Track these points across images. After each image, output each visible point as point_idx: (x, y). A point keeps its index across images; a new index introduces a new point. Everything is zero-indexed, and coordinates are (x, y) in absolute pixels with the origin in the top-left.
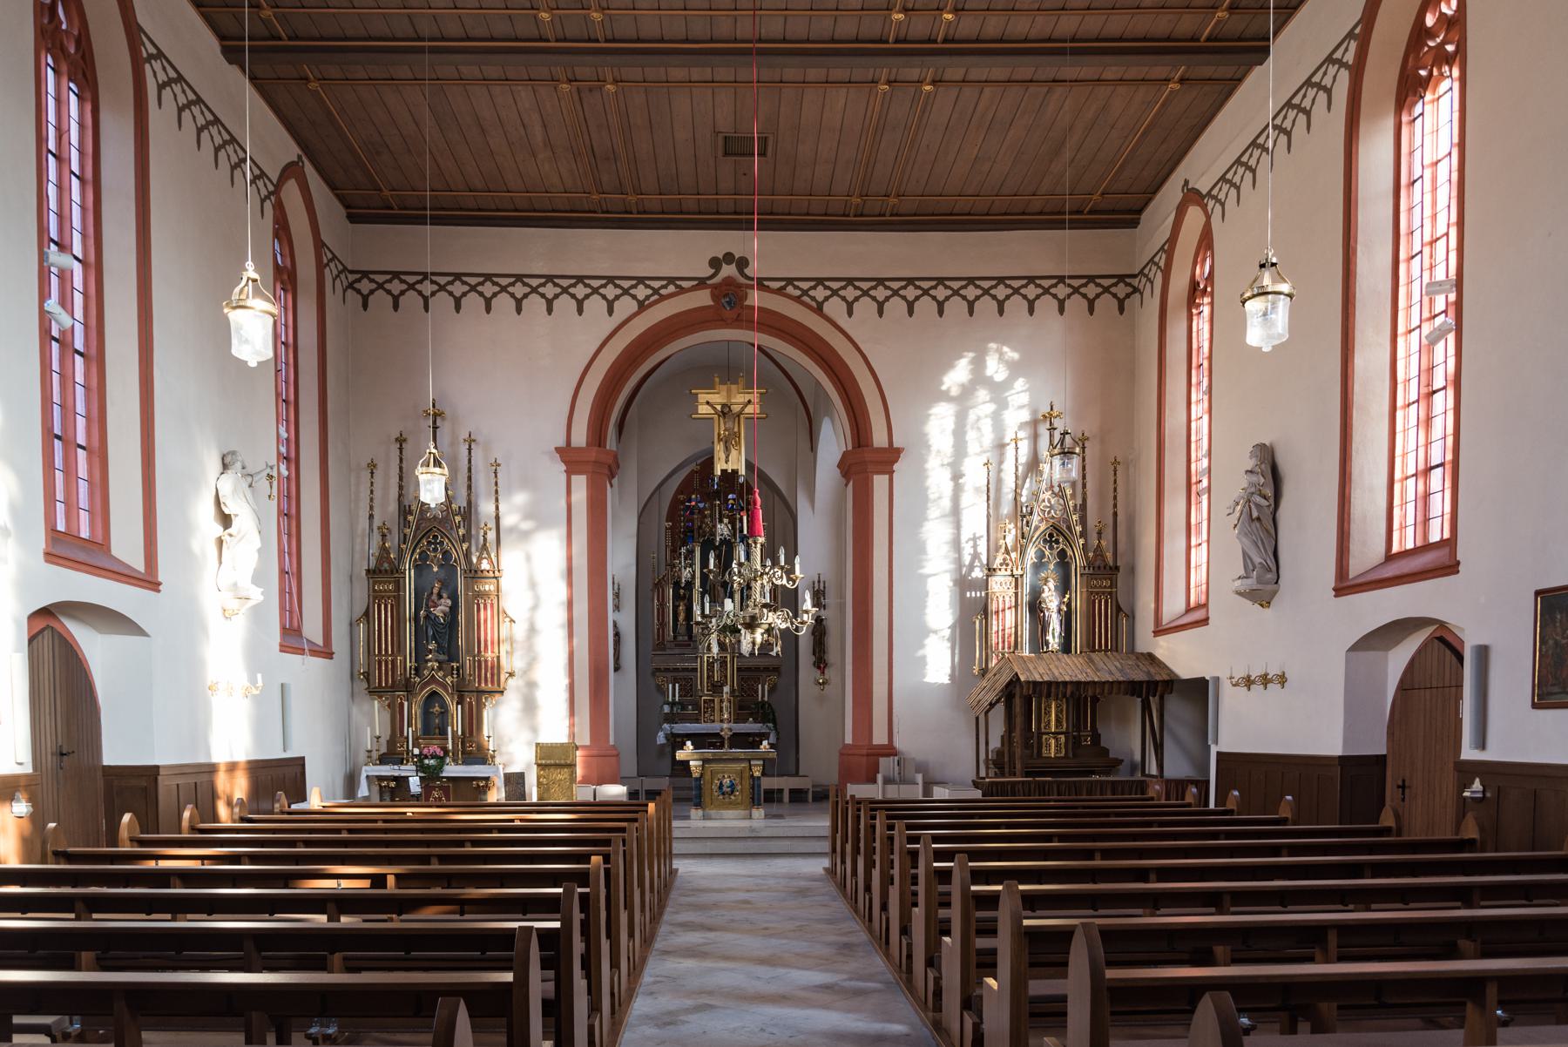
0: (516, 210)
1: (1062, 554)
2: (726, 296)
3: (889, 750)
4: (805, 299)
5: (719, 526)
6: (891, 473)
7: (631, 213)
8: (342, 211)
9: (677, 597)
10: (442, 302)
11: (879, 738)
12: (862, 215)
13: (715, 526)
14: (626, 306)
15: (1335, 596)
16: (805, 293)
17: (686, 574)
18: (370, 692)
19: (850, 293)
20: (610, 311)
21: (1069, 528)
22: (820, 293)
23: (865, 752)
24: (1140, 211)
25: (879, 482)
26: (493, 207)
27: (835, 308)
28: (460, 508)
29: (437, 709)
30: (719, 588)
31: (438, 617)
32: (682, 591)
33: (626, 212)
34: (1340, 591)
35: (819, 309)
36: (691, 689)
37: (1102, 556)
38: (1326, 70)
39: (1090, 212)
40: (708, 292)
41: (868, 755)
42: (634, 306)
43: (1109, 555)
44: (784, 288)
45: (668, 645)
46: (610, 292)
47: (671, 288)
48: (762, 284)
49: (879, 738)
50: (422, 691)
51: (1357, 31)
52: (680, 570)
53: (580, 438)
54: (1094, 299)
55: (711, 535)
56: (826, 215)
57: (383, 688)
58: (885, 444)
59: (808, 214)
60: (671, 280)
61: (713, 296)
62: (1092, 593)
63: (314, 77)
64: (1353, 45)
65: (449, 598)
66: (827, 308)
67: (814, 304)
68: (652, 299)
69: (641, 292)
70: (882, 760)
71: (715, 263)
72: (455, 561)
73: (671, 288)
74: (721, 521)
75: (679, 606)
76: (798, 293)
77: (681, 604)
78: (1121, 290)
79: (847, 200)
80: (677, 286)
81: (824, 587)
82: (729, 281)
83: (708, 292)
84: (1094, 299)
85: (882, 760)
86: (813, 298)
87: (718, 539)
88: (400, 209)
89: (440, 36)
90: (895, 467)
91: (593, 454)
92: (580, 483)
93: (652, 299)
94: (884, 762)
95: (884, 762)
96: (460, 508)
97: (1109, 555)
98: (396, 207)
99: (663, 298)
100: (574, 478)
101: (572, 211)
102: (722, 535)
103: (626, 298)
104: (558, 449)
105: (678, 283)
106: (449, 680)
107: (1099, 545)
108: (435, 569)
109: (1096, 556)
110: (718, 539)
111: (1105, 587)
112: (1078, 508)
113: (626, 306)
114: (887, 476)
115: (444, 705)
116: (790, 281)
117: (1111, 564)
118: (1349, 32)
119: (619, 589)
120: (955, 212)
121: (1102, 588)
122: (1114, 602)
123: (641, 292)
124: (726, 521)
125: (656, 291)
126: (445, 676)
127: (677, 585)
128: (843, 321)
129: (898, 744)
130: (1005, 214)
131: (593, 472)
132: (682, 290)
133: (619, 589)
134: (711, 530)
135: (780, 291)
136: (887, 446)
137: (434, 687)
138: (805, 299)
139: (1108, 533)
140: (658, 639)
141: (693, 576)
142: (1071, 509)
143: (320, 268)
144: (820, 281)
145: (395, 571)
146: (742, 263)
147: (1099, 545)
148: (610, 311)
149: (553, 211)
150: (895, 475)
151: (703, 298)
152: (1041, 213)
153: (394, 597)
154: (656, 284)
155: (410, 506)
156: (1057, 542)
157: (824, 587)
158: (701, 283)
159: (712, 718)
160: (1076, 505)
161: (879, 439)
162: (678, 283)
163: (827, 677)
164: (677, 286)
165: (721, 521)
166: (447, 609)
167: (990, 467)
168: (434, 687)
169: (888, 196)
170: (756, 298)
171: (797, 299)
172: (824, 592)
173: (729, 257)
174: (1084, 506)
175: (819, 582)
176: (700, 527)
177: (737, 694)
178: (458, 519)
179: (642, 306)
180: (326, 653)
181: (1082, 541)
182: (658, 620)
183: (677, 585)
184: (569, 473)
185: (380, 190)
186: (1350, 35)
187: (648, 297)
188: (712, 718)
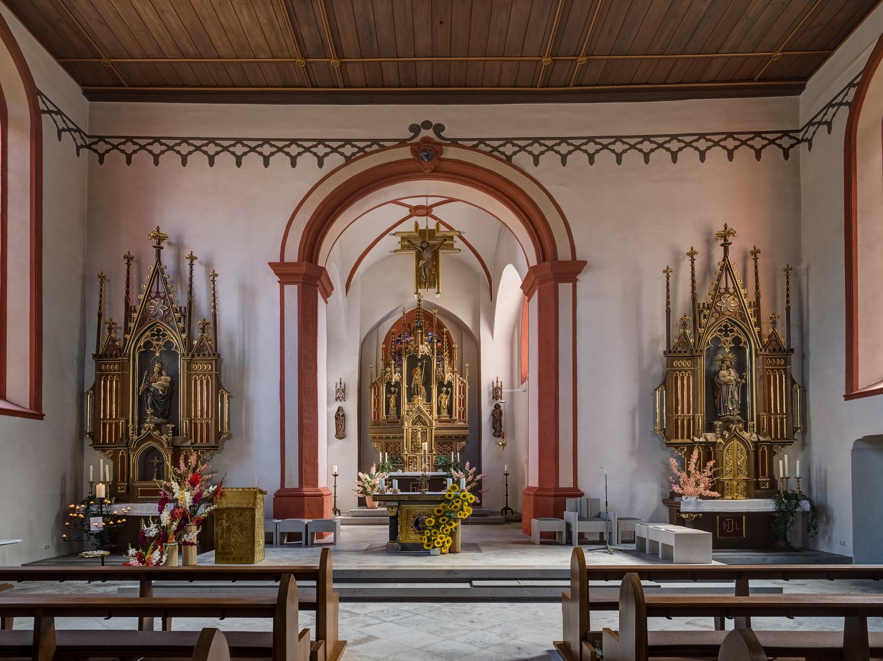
0: (234, 86)
1: (737, 340)
2: (423, 151)
3: (575, 492)
4: (495, 153)
5: (421, 346)
6: (574, 282)
7: (338, 87)
8: (78, 89)
9: (388, 391)
10: (170, 160)
11: (565, 481)
12: (548, 86)
13: (418, 347)
14: (335, 160)
15: (845, 400)
16: (495, 149)
17: (396, 377)
18: (94, 447)
19: (536, 149)
20: (321, 164)
21: (744, 319)
22: (509, 149)
23: (552, 493)
24: (806, 78)
25: (564, 289)
26: (214, 84)
27: (523, 160)
28: (181, 308)
29: (156, 461)
30: (421, 386)
31: (157, 390)
32: (392, 389)
33: (334, 87)
34: (848, 397)
35: (508, 160)
36: (399, 450)
37: (777, 341)
38: (848, 92)
39: (759, 80)
40: (408, 149)
41: (555, 496)
42: (341, 160)
43: (783, 340)
44: (477, 145)
45: (382, 422)
46: (321, 150)
47: (375, 147)
48: (454, 142)
49: (565, 481)
50: (139, 447)
51: (858, 80)
52: (391, 374)
53: (292, 255)
54: (761, 149)
55: (415, 352)
56: (515, 86)
57: (107, 444)
58: (569, 258)
59: (498, 86)
60: (375, 141)
61: (413, 151)
62: (767, 370)
63: (128, 85)
64: (853, 91)
65: (168, 375)
66: (515, 159)
67: (504, 157)
68: (358, 155)
69: (348, 150)
70: (568, 500)
71: (415, 129)
72: (176, 348)
73: (375, 147)
74: (422, 343)
75: (391, 398)
76: (489, 149)
77: (392, 396)
78: (786, 142)
79: (537, 61)
80: (380, 146)
81: (501, 386)
82: (426, 140)
83: (408, 149)
84: (761, 149)
85: (568, 500)
86: (503, 153)
87: (420, 354)
88: (129, 86)
89: (233, 85)
90: (579, 277)
91: (303, 269)
92: (292, 291)
93: (358, 155)
94: (570, 502)
95: (570, 502)
96: (181, 308)
97: (783, 340)
98: (126, 84)
99: (367, 154)
100: (286, 287)
101: (284, 86)
102: (423, 352)
103: (335, 155)
104: (272, 265)
105: (381, 143)
106: (164, 437)
107: (774, 333)
108: (157, 354)
109: (770, 342)
110: (420, 354)
111: (780, 365)
112: (752, 304)
113: (335, 160)
114: (571, 284)
115: (160, 457)
116: (482, 141)
117: (786, 348)
118: (829, 103)
119: (345, 387)
120: (633, 82)
121: (777, 366)
122: (789, 376)
123: (348, 150)
124: (426, 343)
125: (361, 149)
126: (161, 434)
127: (389, 385)
128: (530, 169)
129: (582, 487)
130: (681, 83)
131: (303, 282)
132: (383, 148)
133: (345, 387)
134: (415, 349)
135: (474, 148)
136: (570, 259)
137: (151, 443)
138: (495, 153)
139: (782, 320)
140: (375, 418)
141: (402, 379)
142: (746, 305)
143: (36, 114)
144: (509, 141)
145: (119, 355)
146: (439, 128)
147: (774, 333)
148: (321, 164)
149: (268, 86)
150: (578, 283)
151: (405, 153)
152: (714, 81)
153: (119, 375)
154: (362, 145)
155: (135, 307)
156: (732, 331)
157: (501, 386)
158: (402, 143)
159: (415, 468)
160: (750, 302)
161: (564, 253)
162: (381, 143)
163: (682, 331)
164: (380, 146)
165: (422, 343)
166: (167, 384)
167: (670, 274)
168: (151, 443)
169: (578, 56)
170: (450, 153)
171: (489, 154)
172: (501, 389)
173: (427, 125)
174: (757, 304)
175: (497, 382)
176: (407, 348)
177: (434, 453)
178: (178, 315)
179: (349, 160)
180: (35, 412)
181: (757, 329)
182: (375, 406)
183: (389, 385)
184: (282, 284)
185: (100, 58)
186: (851, 85)
187: (354, 154)
188: (415, 468)
